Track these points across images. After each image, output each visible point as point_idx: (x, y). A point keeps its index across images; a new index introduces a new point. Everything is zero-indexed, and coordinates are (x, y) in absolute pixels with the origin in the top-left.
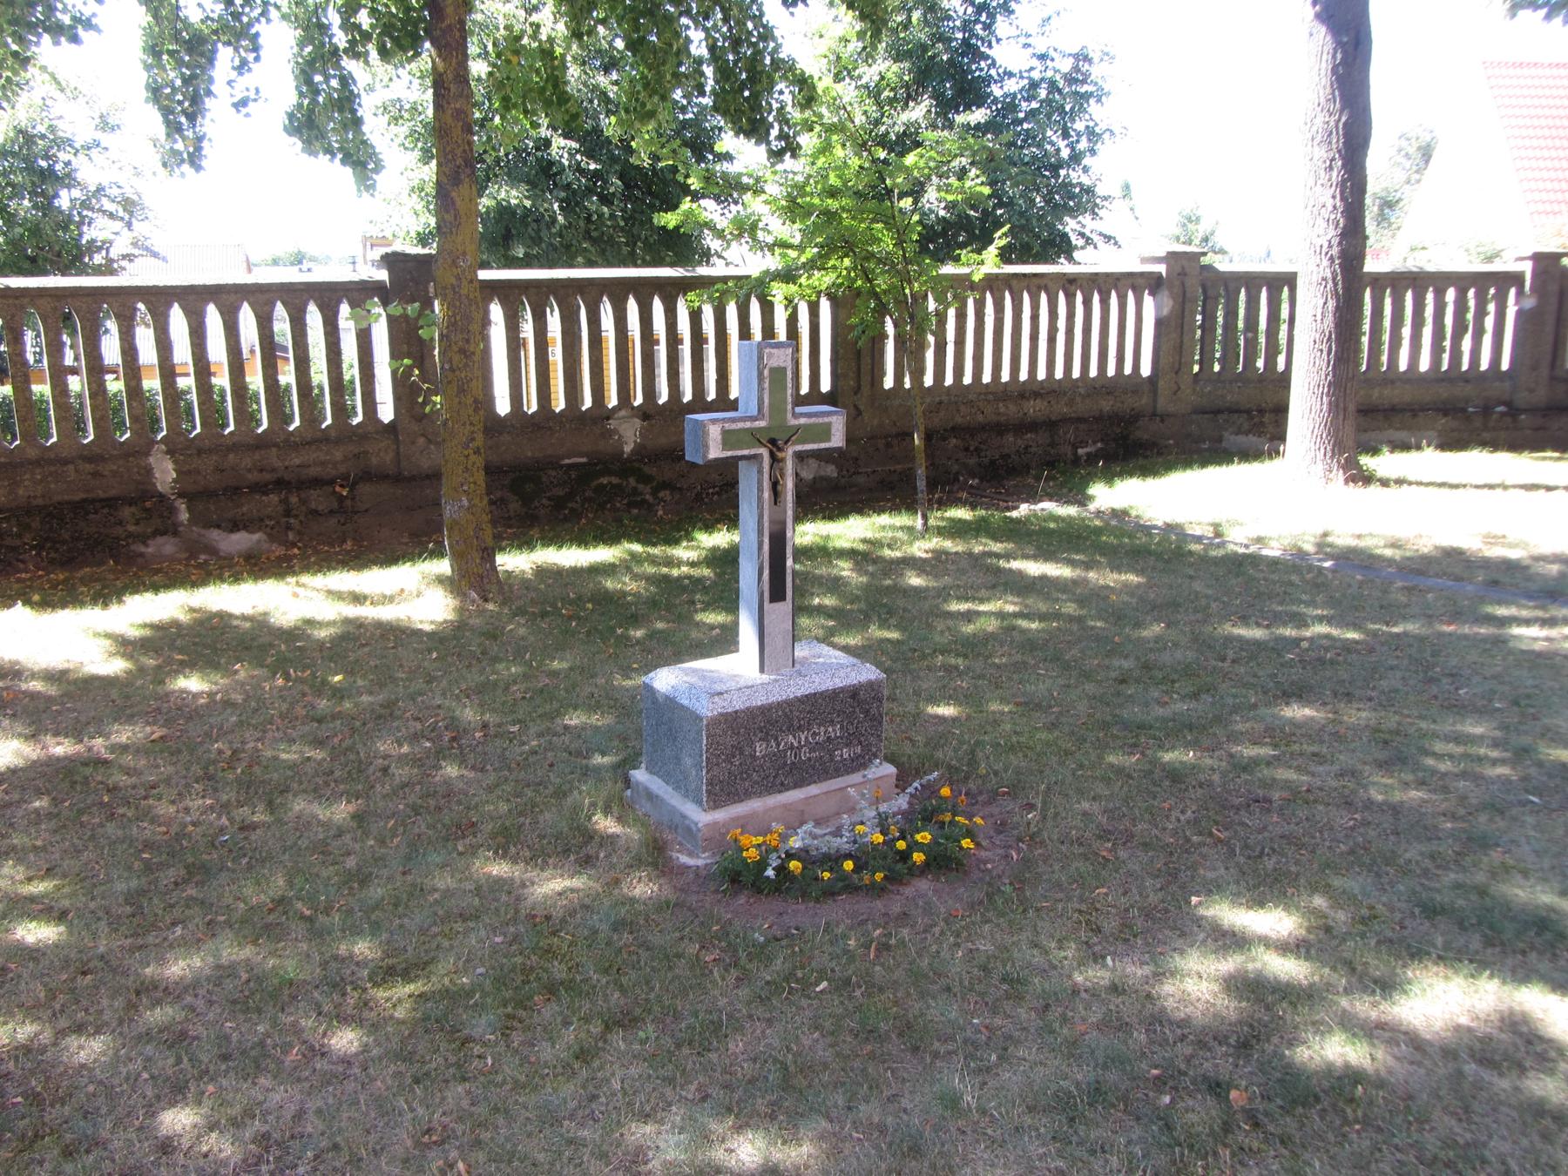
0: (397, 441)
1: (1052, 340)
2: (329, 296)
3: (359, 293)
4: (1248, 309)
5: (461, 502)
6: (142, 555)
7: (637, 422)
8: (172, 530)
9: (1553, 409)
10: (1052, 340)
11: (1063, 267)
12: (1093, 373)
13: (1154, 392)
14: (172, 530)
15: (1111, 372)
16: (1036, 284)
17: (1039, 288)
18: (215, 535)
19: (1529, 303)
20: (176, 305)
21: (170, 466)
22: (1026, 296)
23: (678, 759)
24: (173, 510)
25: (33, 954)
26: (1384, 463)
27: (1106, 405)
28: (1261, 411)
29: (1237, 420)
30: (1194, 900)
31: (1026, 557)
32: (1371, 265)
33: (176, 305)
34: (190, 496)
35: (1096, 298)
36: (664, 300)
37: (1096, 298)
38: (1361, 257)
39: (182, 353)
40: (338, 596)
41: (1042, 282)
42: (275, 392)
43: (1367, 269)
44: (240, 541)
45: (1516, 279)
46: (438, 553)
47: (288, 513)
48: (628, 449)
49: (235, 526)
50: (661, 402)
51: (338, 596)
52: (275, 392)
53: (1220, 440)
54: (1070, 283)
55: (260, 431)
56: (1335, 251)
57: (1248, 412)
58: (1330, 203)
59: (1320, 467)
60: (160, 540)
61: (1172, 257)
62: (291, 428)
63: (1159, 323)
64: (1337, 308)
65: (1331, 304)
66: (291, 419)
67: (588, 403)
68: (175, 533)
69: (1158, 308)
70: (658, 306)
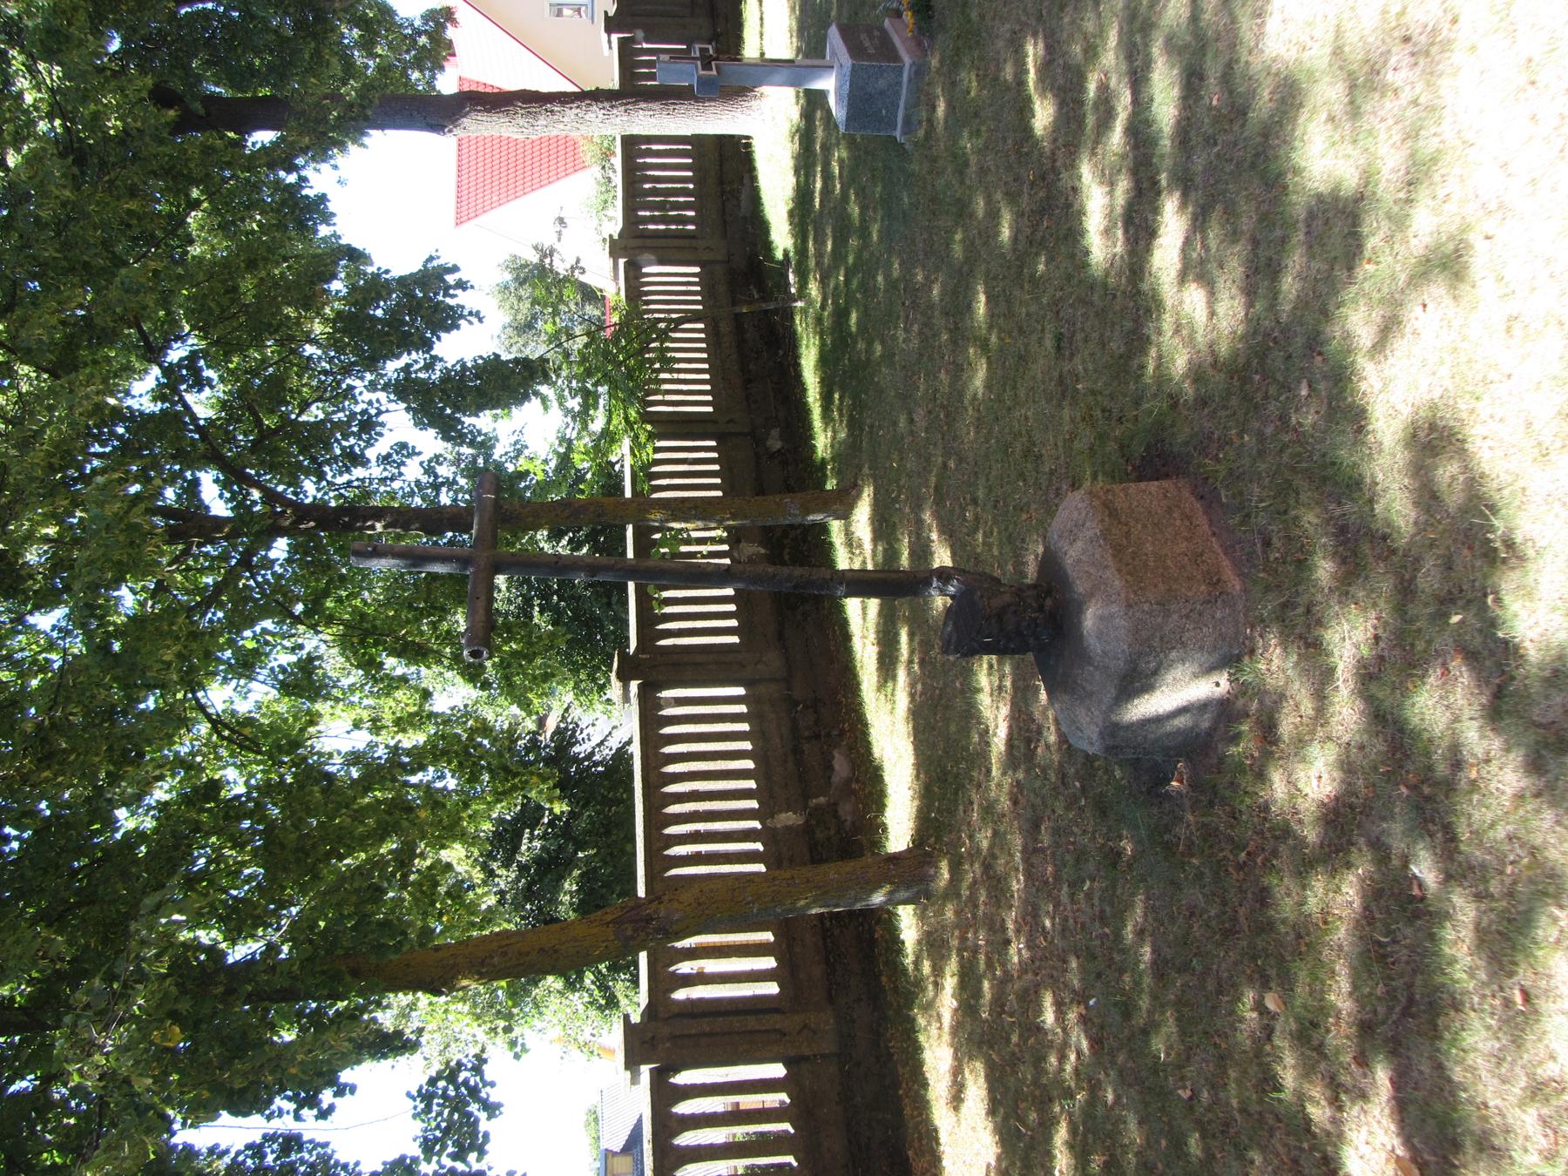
2: (666, 1124)
3: (664, 1095)
5: (789, 511)
6: (853, 823)
8: (833, 808)
9: (713, 13)
11: (635, 749)
13: (713, 262)
14: (833, 808)
17: (658, 754)
18: (835, 779)
19: (640, 34)
20: (672, 1080)
21: (783, 816)
23: (882, 93)
24: (818, 807)
27: (722, 289)
28: (723, 193)
29: (728, 163)
31: (912, 685)
32: (615, 84)
33: (672, 1080)
34: (806, 796)
35: (671, 768)
38: (610, 91)
40: (957, 1100)
43: (617, 87)
44: (841, 766)
45: (623, 44)
46: (824, 529)
47: (817, 737)
48: (763, 551)
49: (829, 767)
51: (957, 1100)
53: (745, 218)
54: (653, 760)
55: (795, 1164)
56: (607, 105)
57: (723, 203)
58: (575, 111)
59: (754, 103)
60: (841, 812)
61: (632, 1063)
62: (795, 1164)
63: (662, 262)
64: (645, 101)
65: (643, 105)
68: (835, 804)
69: (650, 264)
70: (685, 1108)
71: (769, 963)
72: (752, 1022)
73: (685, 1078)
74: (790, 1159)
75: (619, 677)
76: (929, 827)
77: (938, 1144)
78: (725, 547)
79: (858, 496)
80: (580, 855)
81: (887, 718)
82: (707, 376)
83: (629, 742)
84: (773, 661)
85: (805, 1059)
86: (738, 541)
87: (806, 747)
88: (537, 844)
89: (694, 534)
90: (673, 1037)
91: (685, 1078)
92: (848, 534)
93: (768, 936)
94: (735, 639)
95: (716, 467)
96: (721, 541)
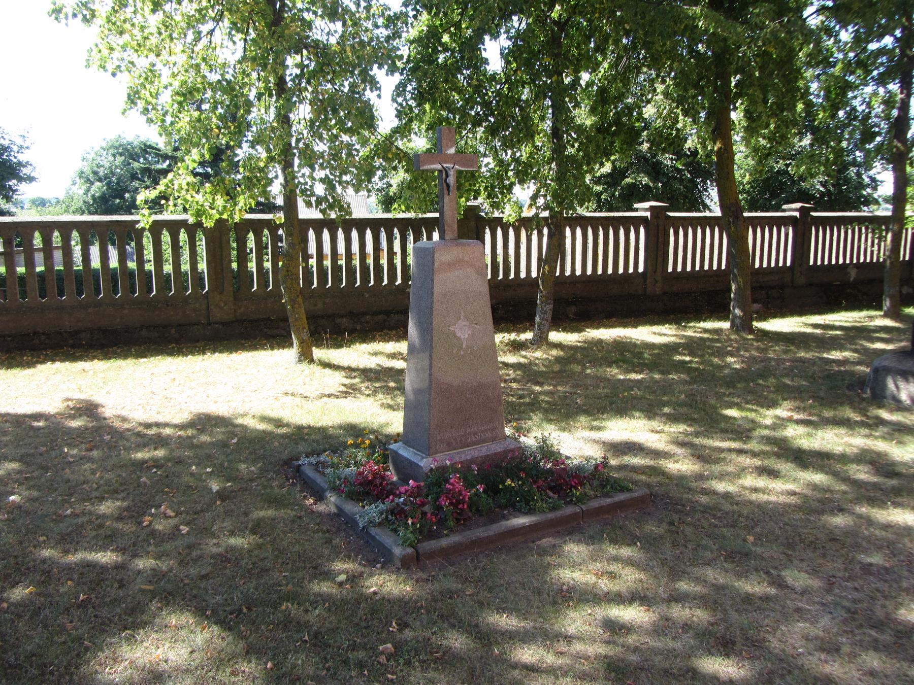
0: (793, 274)
1: (859, 248)
4: (608, 239)
7: (855, 270)
10: (859, 248)
12: (826, 263)
15: (706, 267)
16: (616, 223)
22: (632, 228)
25: (22, 604)
26: (318, 353)
30: (269, 665)
36: (570, 228)
37: (775, 229)
39: (341, 248)
41: (757, 221)
42: (336, 268)
46: (402, 334)
48: (852, 279)
50: (397, 284)
52: (336, 268)
62: (397, 284)
66: (187, 289)
67: (512, 276)
71: (578, 272)
72: (660, 259)
73: (642, 231)
74: (372, 283)
75: (802, 207)
76: (765, 334)
77: (220, 352)
78: (855, 261)
79: (896, 322)
80: (660, 185)
81: (793, 324)
82: (589, 272)
83: (710, 211)
84: (801, 280)
85: (645, 281)
86: (857, 268)
87: (763, 292)
88: (669, 163)
89: (883, 244)
90: (658, 226)
91: (642, 231)
92: (876, 317)
93: (723, 267)
94: (811, 263)
95: (600, 272)
96: (878, 258)
